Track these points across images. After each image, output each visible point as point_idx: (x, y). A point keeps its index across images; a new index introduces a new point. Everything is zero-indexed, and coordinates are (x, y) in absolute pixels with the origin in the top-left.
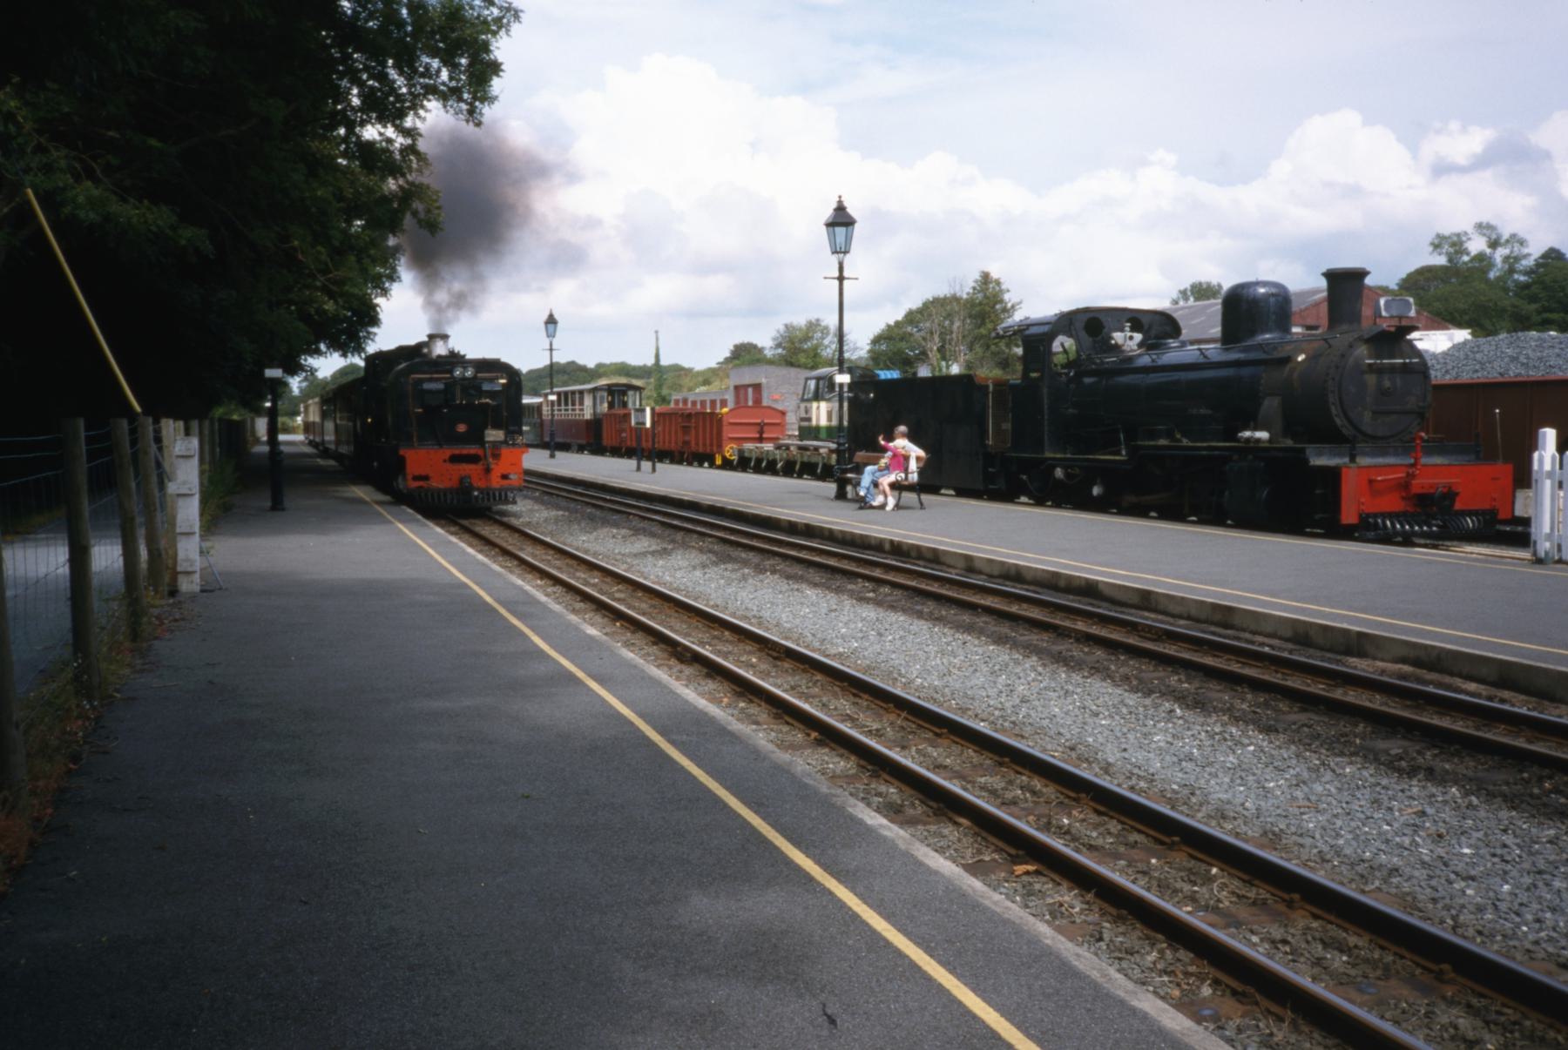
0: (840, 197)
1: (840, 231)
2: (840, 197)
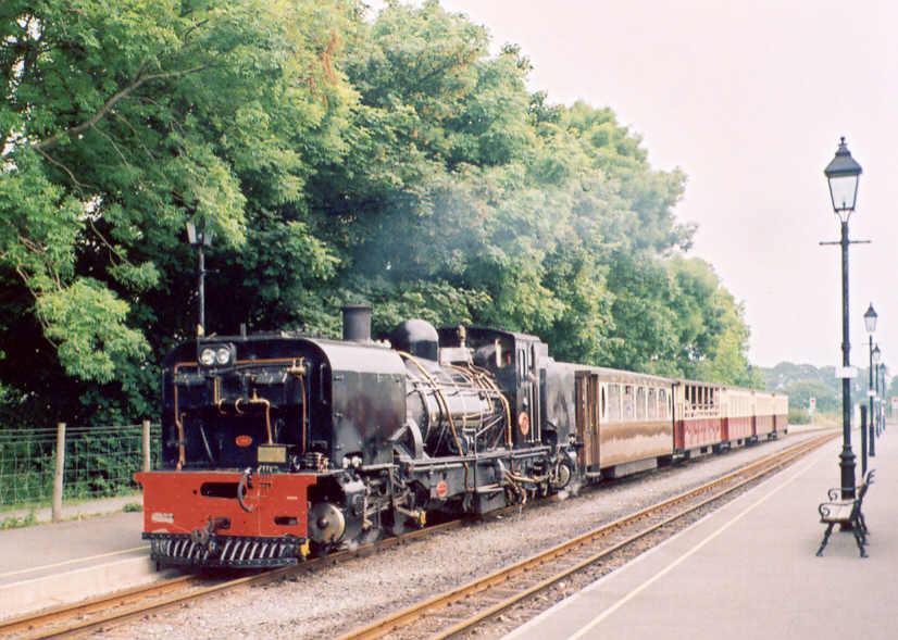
0: (843, 139)
1: (844, 184)
2: (843, 139)
